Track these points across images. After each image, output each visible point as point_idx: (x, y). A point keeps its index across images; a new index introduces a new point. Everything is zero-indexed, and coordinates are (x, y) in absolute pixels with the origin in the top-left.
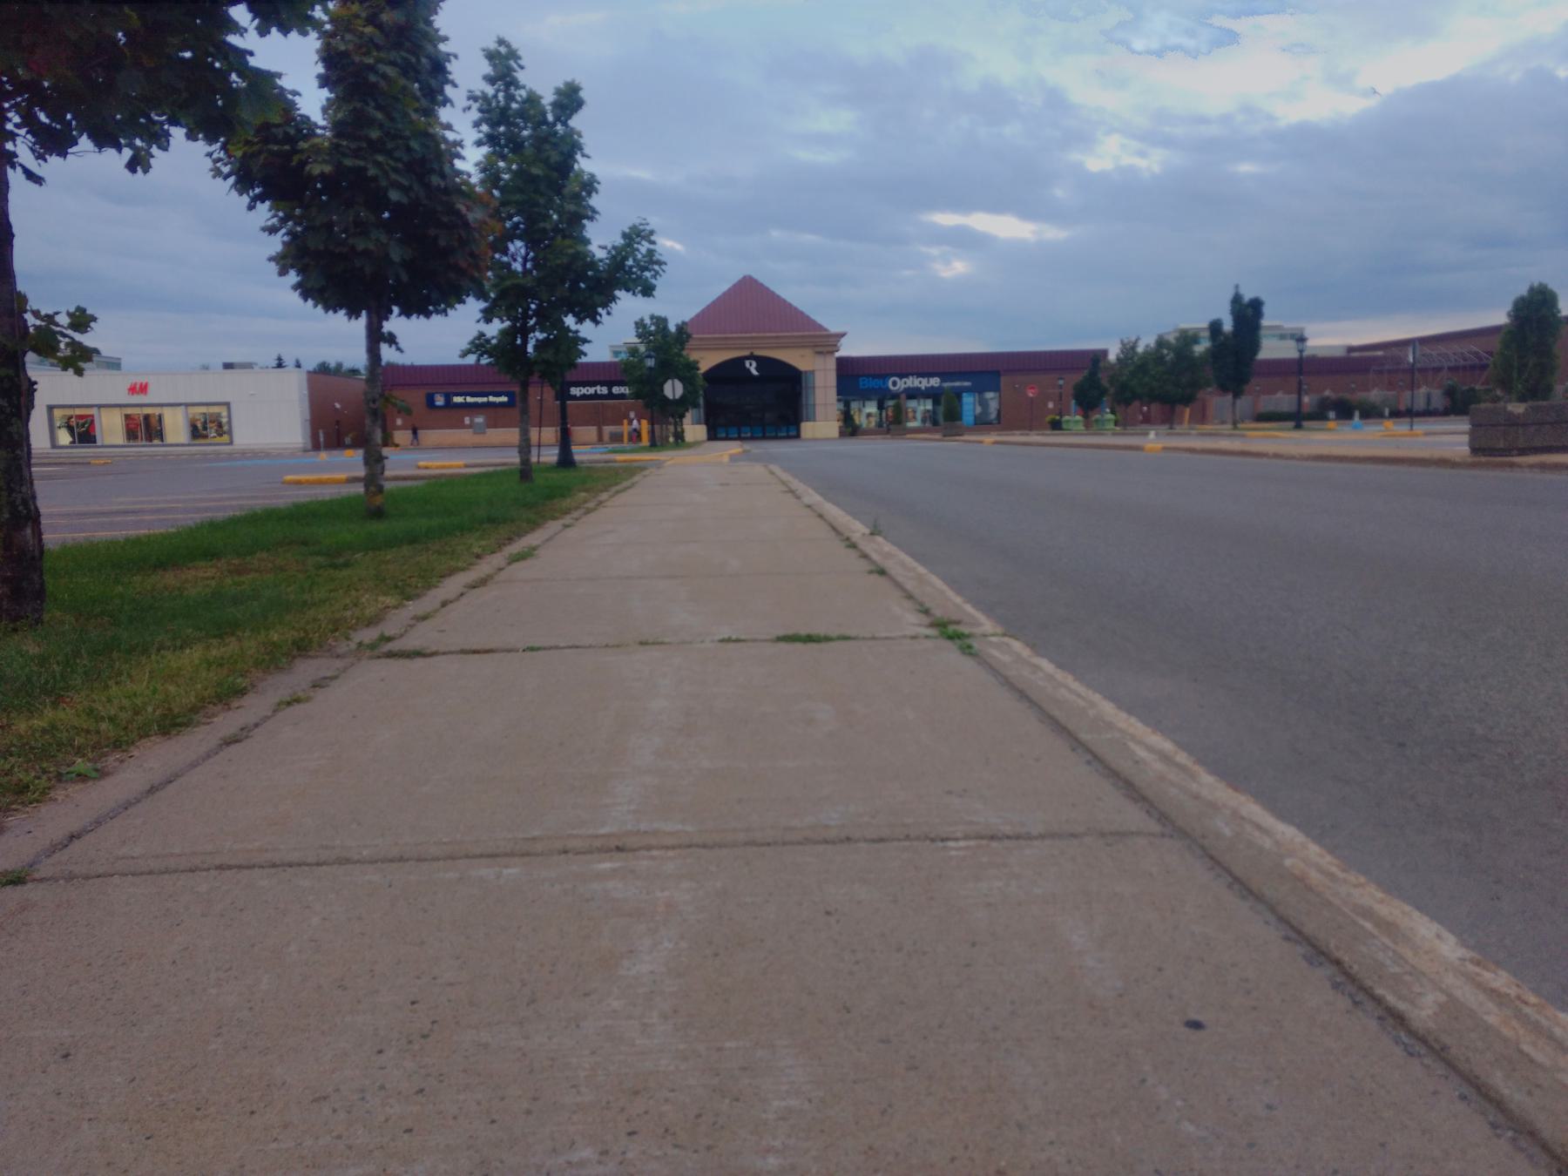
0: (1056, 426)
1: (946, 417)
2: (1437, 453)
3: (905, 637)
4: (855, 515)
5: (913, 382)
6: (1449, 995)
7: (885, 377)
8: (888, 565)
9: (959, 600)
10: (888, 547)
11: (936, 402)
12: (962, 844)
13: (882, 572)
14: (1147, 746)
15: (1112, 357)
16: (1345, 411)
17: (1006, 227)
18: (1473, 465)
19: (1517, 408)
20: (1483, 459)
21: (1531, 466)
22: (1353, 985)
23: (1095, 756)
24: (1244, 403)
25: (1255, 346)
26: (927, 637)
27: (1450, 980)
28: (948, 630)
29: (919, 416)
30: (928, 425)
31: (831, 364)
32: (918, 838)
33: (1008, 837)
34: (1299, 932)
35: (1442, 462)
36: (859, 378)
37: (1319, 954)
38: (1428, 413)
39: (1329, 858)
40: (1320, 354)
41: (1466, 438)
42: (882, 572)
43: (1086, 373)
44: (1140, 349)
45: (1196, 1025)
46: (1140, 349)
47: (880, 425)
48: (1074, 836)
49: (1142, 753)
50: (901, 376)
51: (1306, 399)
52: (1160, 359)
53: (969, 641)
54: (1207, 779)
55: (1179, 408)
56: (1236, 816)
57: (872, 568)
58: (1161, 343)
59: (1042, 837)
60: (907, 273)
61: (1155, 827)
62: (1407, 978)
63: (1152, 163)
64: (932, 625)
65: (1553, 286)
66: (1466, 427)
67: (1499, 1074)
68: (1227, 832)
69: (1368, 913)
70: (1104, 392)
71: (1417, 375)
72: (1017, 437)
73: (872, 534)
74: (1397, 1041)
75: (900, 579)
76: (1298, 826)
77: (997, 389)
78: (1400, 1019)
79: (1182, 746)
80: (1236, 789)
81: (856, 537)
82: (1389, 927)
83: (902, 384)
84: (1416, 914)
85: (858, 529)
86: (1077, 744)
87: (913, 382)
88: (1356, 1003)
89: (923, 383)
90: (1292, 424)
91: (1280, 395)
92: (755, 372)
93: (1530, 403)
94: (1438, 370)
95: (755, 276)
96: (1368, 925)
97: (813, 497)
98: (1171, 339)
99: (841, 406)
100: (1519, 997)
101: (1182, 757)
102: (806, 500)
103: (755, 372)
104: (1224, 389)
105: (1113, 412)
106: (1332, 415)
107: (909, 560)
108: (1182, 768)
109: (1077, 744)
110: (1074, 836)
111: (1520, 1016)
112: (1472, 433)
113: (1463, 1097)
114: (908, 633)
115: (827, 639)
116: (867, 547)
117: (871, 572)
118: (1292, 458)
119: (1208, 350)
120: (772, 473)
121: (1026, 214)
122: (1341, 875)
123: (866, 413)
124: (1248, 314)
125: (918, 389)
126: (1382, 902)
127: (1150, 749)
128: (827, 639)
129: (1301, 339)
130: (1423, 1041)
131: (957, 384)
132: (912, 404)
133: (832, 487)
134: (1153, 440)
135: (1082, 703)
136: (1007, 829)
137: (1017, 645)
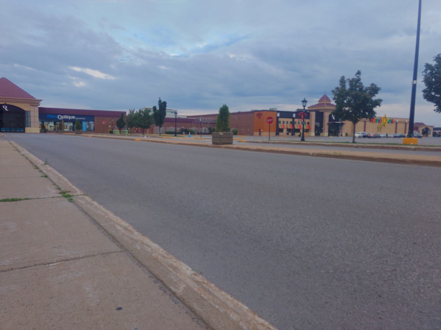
0: (111, 132)
1: (77, 128)
2: (205, 144)
3: (50, 197)
4: (40, 158)
5: (66, 117)
6: (187, 285)
7: (57, 115)
8: (49, 174)
9: (71, 185)
10: (50, 168)
11: (74, 124)
12: (55, 264)
13: (46, 177)
14: (120, 225)
15: (127, 114)
16: (187, 132)
17: (97, 74)
18: (213, 147)
19: (221, 134)
20: (215, 145)
21: (224, 147)
22: (165, 287)
23: (105, 230)
24: (162, 129)
25: (165, 114)
26: (58, 197)
27: (188, 280)
28: (66, 195)
29: (68, 127)
30: (71, 130)
31: (37, 109)
32: (39, 265)
33: (72, 259)
34: (153, 274)
35: (207, 146)
36: (46, 115)
37: (158, 280)
38: (205, 134)
39: (164, 252)
40: (181, 117)
41: (211, 140)
42: (46, 177)
43: (120, 118)
44: (135, 113)
45: (120, 309)
46: (135, 113)
47: (55, 129)
48: (94, 256)
49: (119, 228)
50: (62, 115)
51: (178, 129)
52: (140, 115)
53: (72, 198)
54: (136, 233)
55: (145, 129)
56: (142, 243)
57: (43, 175)
58: (140, 111)
59: (83, 257)
60: (64, 84)
61: (119, 249)
62: (178, 282)
63: (139, 63)
64: (60, 193)
65: (228, 105)
66: (211, 137)
67: (195, 304)
68: (139, 248)
69: (171, 266)
70: (125, 124)
71: (202, 124)
72: (100, 135)
73: (45, 164)
74: (173, 300)
75: (52, 179)
76: (160, 245)
77: (93, 121)
78: (174, 294)
79: (131, 224)
80: (143, 236)
81: (38, 165)
82: (175, 269)
83: (62, 117)
84: (183, 264)
85: (40, 163)
86: (100, 227)
87: (66, 117)
88: (165, 292)
89: (70, 118)
90: (174, 135)
91: (171, 127)
92: (7, 110)
93: (224, 132)
94: (207, 123)
95: (7, 78)
96: (171, 269)
97: (25, 152)
98: (143, 110)
99: (41, 123)
100: (203, 282)
101: (131, 228)
102: (23, 153)
103: (7, 110)
104: (157, 125)
105: (128, 129)
106: (184, 133)
107: (56, 172)
108: (130, 231)
109: (100, 227)
110: (94, 256)
111: (203, 287)
112: (213, 139)
113: (187, 312)
114: (51, 196)
115: (20, 200)
116: (43, 169)
117: (42, 177)
118: (173, 144)
119: (152, 114)
120: (11, 144)
121: (103, 70)
122: (167, 256)
123: (50, 125)
124: (163, 105)
125: (68, 119)
126: (175, 262)
127: (121, 226)
128: (20, 200)
129: (176, 113)
130: (179, 299)
131: (81, 118)
132: (66, 124)
133: (33, 149)
134: (139, 138)
135: (104, 214)
136: (72, 257)
137: (87, 198)
